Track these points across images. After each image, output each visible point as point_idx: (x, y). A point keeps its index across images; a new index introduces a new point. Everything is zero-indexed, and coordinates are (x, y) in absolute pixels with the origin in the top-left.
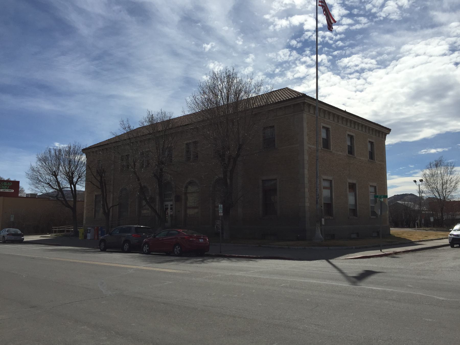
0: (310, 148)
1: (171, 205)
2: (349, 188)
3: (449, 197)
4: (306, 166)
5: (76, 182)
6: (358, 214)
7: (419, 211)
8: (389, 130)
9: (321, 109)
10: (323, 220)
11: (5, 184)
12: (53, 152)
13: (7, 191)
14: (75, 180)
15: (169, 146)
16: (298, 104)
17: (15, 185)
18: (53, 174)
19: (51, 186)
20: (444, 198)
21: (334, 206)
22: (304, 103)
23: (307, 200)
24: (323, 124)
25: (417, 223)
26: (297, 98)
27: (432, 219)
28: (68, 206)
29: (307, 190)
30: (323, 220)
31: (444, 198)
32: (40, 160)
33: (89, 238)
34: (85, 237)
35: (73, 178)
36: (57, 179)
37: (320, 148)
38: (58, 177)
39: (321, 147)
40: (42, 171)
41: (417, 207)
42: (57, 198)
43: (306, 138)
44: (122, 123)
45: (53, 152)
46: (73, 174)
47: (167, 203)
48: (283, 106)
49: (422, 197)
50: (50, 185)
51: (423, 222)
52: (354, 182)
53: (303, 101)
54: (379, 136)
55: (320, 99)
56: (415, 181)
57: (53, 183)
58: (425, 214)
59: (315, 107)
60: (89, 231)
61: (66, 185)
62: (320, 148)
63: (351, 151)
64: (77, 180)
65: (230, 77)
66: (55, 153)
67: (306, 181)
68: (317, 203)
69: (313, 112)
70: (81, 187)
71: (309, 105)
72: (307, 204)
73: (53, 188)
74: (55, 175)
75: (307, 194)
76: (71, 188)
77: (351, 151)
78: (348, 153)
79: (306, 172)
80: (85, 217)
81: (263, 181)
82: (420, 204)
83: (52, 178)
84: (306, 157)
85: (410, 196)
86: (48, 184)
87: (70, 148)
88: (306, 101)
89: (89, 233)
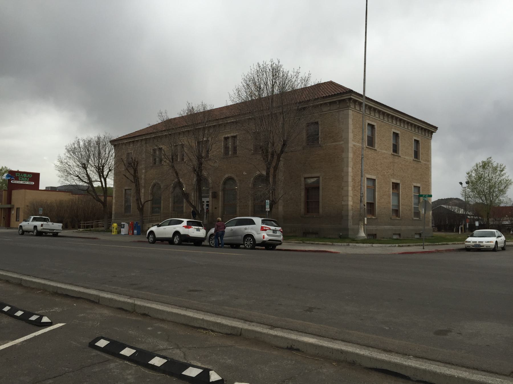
0: (354, 145)
1: (207, 202)
2: (393, 189)
3: (497, 201)
4: (351, 164)
5: (107, 176)
6: (377, 212)
7: (464, 216)
8: (436, 128)
9: (367, 105)
10: (366, 219)
11: (25, 175)
12: (82, 143)
13: (27, 183)
14: (105, 173)
15: (205, 139)
16: (344, 100)
17: (35, 177)
18: (83, 167)
19: (81, 179)
20: (491, 201)
21: (377, 205)
22: (350, 99)
23: (350, 199)
24: (368, 122)
25: (461, 228)
26: (344, 93)
27: (477, 224)
28: (99, 200)
29: (350, 188)
30: (366, 219)
31: (491, 201)
32: (69, 151)
33: (122, 233)
34: (119, 232)
35: (103, 172)
36: (87, 171)
37: (365, 146)
38: (88, 169)
39: (366, 144)
40: (71, 162)
41: (461, 211)
42: (88, 192)
43: (351, 135)
44: (160, 114)
45: (82, 143)
46: (103, 167)
47: (203, 199)
48: (328, 101)
49: (468, 202)
50: (79, 178)
51: (468, 227)
52: (398, 182)
53: (349, 97)
54: (425, 134)
55: (367, 95)
56: (461, 183)
57: (83, 175)
58: (471, 219)
59: (360, 104)
60: (123, 226)
61: (94, 176)
62: (365, 146)
63: (395, 149)
64: (108, 173)
65: (275, 71)
66: (85, 144)
67: (350, 179)
68: (361, 201)
69: (359, 109)
70: (110, 183)
71: (355, 101)
72: (350, 203)
73: (83, 181)
74: (85, 167)
75: (351, 193)
76: (101, 181)
77: (395, 149)
78: (393, 152)
79: (350, 169)
80: (113, 212)
81: (305, 178)
82: (465, 210)
83: (82, 170)
84: (351, 155)
85: (456, 201)
86: (78, 176)
87: (99, 138)
88: (352, 97)
89: (124, 228)
